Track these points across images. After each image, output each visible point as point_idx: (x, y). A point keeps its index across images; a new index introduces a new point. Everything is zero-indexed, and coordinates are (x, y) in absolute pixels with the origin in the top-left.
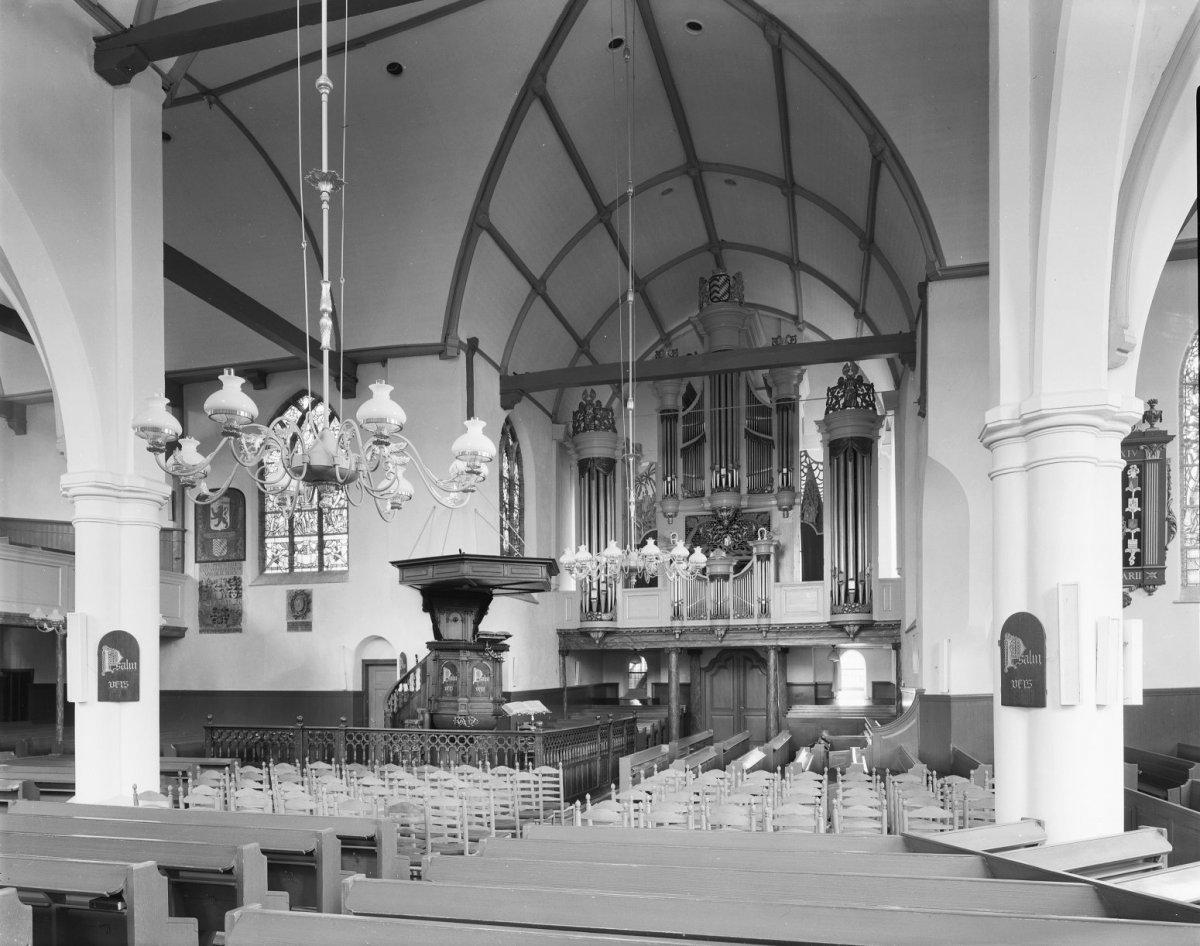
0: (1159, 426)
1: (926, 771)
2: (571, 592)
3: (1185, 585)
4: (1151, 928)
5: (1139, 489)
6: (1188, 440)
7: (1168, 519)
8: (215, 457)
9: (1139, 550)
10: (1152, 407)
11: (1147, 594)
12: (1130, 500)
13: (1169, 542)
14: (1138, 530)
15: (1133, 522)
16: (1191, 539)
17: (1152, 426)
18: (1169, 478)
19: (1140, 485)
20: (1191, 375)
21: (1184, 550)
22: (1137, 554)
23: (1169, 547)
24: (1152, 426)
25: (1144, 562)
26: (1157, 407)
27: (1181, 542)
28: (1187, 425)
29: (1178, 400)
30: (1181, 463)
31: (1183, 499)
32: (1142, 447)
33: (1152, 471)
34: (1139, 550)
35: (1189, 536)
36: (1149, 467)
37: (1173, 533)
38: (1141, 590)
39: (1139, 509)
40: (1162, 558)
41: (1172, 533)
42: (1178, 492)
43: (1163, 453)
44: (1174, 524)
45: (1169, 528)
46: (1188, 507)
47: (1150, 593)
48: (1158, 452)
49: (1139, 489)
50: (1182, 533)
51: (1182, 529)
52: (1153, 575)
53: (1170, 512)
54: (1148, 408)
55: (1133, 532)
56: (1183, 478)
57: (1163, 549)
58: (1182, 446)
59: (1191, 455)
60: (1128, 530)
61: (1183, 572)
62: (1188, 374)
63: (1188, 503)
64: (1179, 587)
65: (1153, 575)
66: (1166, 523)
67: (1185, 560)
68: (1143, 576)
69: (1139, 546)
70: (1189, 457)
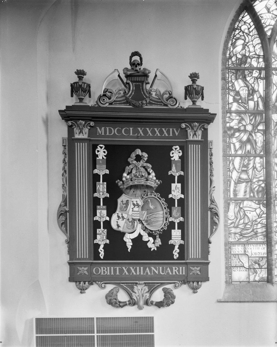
0: (201, 104)
1: (273, 24)
2: (266, 202)
3: (229, 282)
4: (130, 124)
5: (182, 173)
6: (231, 128)
7: (211, 209)
8: (151, 203)
9: (182, 242)
10: (194, 81)
11: (191, 291)
12: (98, 231)
13: (212, 233)
14: (182, 219)
15: (176, 210)
16: (235, 234)
17: (194, 102)
18: (211, 163)
19: (183, 169)
20: (234, 59)
21: (228, 245)
22: (181, 247)
23: (212, 239)
24: (194, 102)
25: (188, 256)
26: (199, 82)
27: (225, 235)
28: (231, 112)
29: (220, 83)
30: (224, 151)
31: (227, 190)
32: (183, 125)
33: (194, 152)
34: (182, 242)
35: (233, 230)
36: (191, 147)
37: (216, 224)
38: (185, 287)
39: (183, 196)
40: (205, 252)
41: (214, 224)
42: (222, 182)
43: (205, 133)
44: (216, 214)
45: (212, 218)
46: (231, 199)
47: (195, 290)
48: (199, 133)
49: (182, 173)
50: (225, 226)
51: (226, 221)
52: (196, 270)
53: (212, 201)
54: (191, 83)
55: (177, 221)
56: (227, 170)
57: (206, 242)
58: (225, 132)
59: (234, 144)
60: (171, 219)
61: (226, 268)
62: (231, 58)
63: (232, 196)
64: (223, 285)
65: (196, 270)
66: (209, 212)
67: (228, 255)
68: (187, 270)
69: (183, 238)
70: (232, 145)
